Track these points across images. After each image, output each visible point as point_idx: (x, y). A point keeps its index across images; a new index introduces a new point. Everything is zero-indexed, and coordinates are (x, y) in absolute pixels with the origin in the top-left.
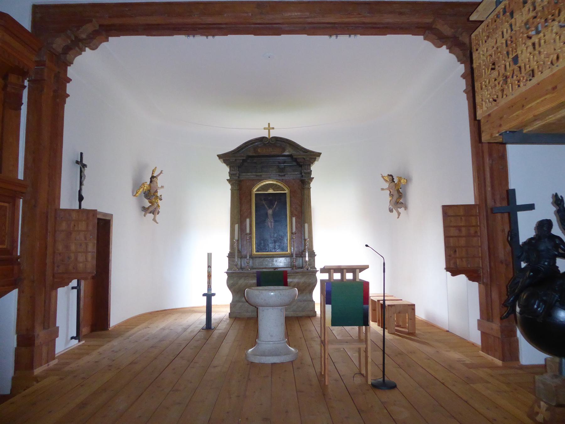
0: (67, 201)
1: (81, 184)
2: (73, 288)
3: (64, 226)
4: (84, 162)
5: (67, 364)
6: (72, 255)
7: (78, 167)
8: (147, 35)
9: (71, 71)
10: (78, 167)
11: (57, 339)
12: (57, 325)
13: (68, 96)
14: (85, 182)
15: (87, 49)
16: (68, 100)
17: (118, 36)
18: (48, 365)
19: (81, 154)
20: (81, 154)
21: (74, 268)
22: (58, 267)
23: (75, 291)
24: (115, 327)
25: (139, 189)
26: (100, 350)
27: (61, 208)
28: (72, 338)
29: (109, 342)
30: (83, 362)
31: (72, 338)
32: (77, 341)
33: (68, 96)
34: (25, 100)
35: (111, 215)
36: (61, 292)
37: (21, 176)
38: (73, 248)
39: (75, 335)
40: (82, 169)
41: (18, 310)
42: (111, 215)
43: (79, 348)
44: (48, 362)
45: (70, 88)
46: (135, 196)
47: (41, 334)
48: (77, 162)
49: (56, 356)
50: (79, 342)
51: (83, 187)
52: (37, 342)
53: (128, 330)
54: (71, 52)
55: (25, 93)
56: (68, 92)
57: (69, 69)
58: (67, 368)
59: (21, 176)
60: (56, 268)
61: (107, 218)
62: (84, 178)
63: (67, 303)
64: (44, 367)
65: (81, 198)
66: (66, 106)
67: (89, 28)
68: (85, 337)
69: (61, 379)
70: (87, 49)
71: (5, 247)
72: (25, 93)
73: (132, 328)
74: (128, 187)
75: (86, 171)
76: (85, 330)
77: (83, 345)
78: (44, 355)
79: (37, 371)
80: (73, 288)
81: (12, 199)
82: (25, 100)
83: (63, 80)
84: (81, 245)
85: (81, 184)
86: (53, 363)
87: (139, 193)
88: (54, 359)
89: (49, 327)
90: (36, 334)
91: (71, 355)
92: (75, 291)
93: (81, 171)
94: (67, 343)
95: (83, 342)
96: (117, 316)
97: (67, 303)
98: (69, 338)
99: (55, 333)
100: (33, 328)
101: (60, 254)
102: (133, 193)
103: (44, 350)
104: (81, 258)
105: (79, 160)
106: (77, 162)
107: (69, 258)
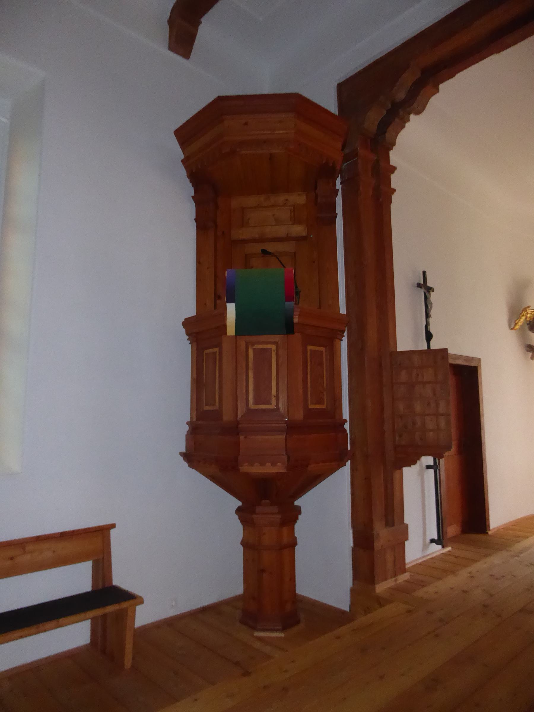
0: (407, 338)
1: (428, 316)
2: (428, 467)
3: (403, 376)
4: (429, 284)
5: (423, 584)
6: (418, 420)
7: (422, 292)
8: (499, 51)
9: (394, 157)
10: (422, 292)
11: (407, 543)
12: (406, 522)
13: (394, 191)
14: (432, 313)
15: (412, 117)
16: (394, 197)
17: (452, 76)
18: (396, 581)
19: (424, 273)
20: (424, 273)
21: (421, 439)
22: (400, 436)
23: (432, 471)
24: (498, 529)
25: (519, 318)
26: (473, 568)
27: (398, 350)
28: (432, 541)
29: (487, 555)
30: (451, 582)
31: (432, 541)
32: (440, 547)
33: (394, 191)
34: (339, 209)
35: (479, 360)
36: (409, 474)
37: (343, 310)
38: (418, 407)
39: (436, 538)
40: (427, 294)
41: (353, 494)
42: (479, 360)
43: (442, 558)
44: (395, 575)
45: (395, 180)
46: (513, 329)
47: (382, 534)
48: (419, 285)
49: (407, 567)
50: (443, 547)
51: (431, 320)
52: (378, 545)
53: (518, 538)
54: (390, 129)
55: (339, 200)
56: (393, 186)
57: (391, 153)
58: (420, 593)
59: (343, 310)
60: (397, 438)
61: (473, 364)
62: (431, 307)
63: (419, 489)
64: (390, 583)
65: (429, 336)
66: (393, 207)
67: (408, 78)
68: (454, 540)
69: (409, 611)
70: (412, 117)
71: (324, 407)
72: (339, 200)
73: (526, 537)
74: (503, 318)
75: (433, 297)
76: (452, 530)
77: (449, 554)
78: (390, 566)
79: (381, 588)
80: (428, 467)
81: (330, 340)
82: (339, 209)
83: (383, 172)
84: (429, 404)
85: (428, 316)
86: (403, 578)
87: (520, 324)
88: (404, 571)
89: (393, 525)
90: (375, 533)
91: (431, 569)
92: (432, 471)
93: (426, 298)
94: (425, 547)
95: (449, 548)
96: (500, 512)
97: (419, 489)
98: (428, 541)
99: (403, 534)
100: (371, 520)
101: (401, 417)
102: (510, 326)
103: (389, 557)
104: (430, 424)
105: (422, 282)
106: (419, 285)
107: (414, 423)
